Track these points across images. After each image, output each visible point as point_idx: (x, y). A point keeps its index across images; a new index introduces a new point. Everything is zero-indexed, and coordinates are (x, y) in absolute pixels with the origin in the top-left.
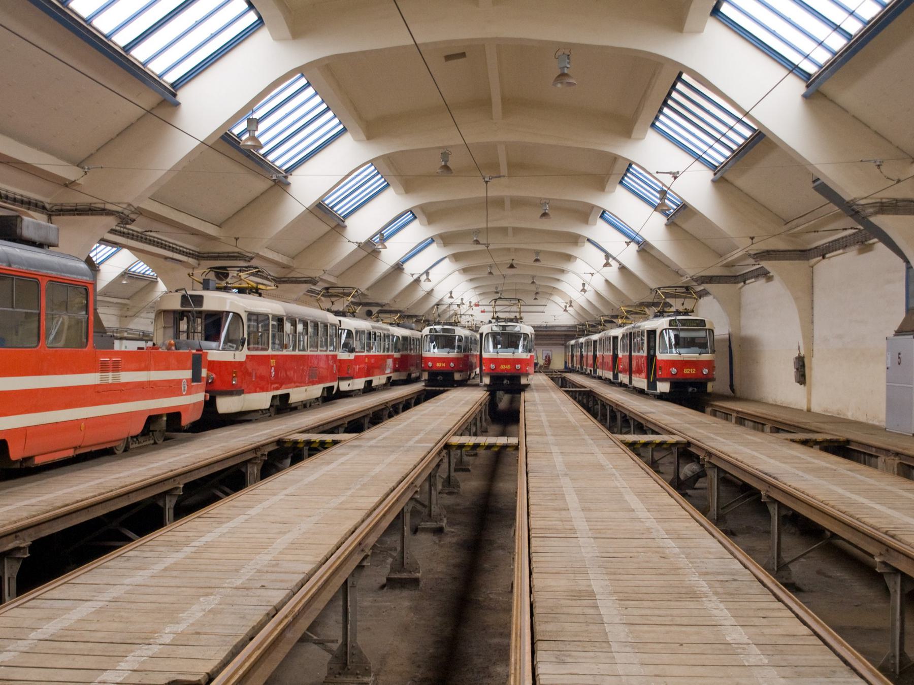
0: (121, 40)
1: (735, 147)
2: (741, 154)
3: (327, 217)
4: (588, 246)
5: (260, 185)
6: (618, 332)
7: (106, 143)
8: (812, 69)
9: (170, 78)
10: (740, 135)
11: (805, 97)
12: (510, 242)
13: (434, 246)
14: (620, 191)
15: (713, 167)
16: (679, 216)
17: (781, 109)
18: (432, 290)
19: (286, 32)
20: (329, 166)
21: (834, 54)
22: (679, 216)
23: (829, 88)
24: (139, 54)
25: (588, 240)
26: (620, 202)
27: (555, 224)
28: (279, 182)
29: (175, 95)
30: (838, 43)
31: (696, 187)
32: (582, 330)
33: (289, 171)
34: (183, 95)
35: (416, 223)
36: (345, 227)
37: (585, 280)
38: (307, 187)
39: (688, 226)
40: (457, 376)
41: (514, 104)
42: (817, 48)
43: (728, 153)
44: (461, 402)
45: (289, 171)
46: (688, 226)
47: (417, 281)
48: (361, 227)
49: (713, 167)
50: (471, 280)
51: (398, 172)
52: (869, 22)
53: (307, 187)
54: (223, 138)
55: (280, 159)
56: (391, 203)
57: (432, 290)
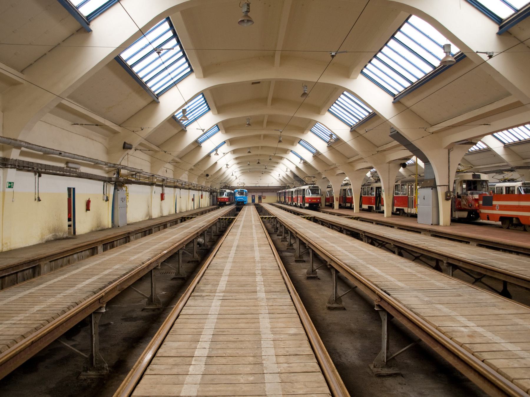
0: (130, 63)
1: (361, 119)
2: (364, 122)
3: (176, 125)
4: (291, 153)
5: (141, 102)
6: (293, 190)
7: (42, 56)
8: (396, 93)
9: (156, 93)
10: (363, 114)
11: (498, 34)
12: (259, 152)
13: (225, 145)
14: (298, 145)
15: (350, 126)
16: (317, 155)
17: (383, 105)
18: (216, 163)
19: (202, 75)
20: (180, 90)
21: (517, 11)
22: (317, 155)
23: (403, 100)
24: (135, 69)
25: (291, 151)
26: (298, 148)
27: (281, 146)
28: (154, 100)
29: (88, 24)
30: (429, 70)
31: (343, 133)
32: (284, 187)
33: (159, 95)
34: (95, 25)
35: (220, 133)
36: (186, 131)
37: (276, 176)
38: (169, 105)
39: (337, 147)
40: (227, 203)
41: (276, 100)
42: (399, 86)
43: (367, 114)
44: (233, 207)
45: (159, 95)
46: (337, 147)
47: (209, 156)
48: (193, 133)
49: (350, 126)
50: (238, 163)
51: (215, 99)
52: (455, 55)
53: (169, 105)
54: (116, 58)
55: (155, 86)
56: (210, 120)
57: (216, 163)
